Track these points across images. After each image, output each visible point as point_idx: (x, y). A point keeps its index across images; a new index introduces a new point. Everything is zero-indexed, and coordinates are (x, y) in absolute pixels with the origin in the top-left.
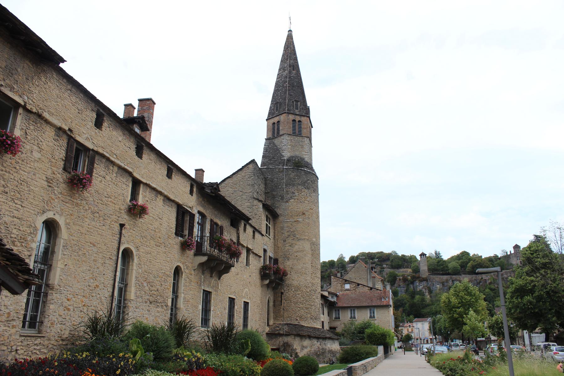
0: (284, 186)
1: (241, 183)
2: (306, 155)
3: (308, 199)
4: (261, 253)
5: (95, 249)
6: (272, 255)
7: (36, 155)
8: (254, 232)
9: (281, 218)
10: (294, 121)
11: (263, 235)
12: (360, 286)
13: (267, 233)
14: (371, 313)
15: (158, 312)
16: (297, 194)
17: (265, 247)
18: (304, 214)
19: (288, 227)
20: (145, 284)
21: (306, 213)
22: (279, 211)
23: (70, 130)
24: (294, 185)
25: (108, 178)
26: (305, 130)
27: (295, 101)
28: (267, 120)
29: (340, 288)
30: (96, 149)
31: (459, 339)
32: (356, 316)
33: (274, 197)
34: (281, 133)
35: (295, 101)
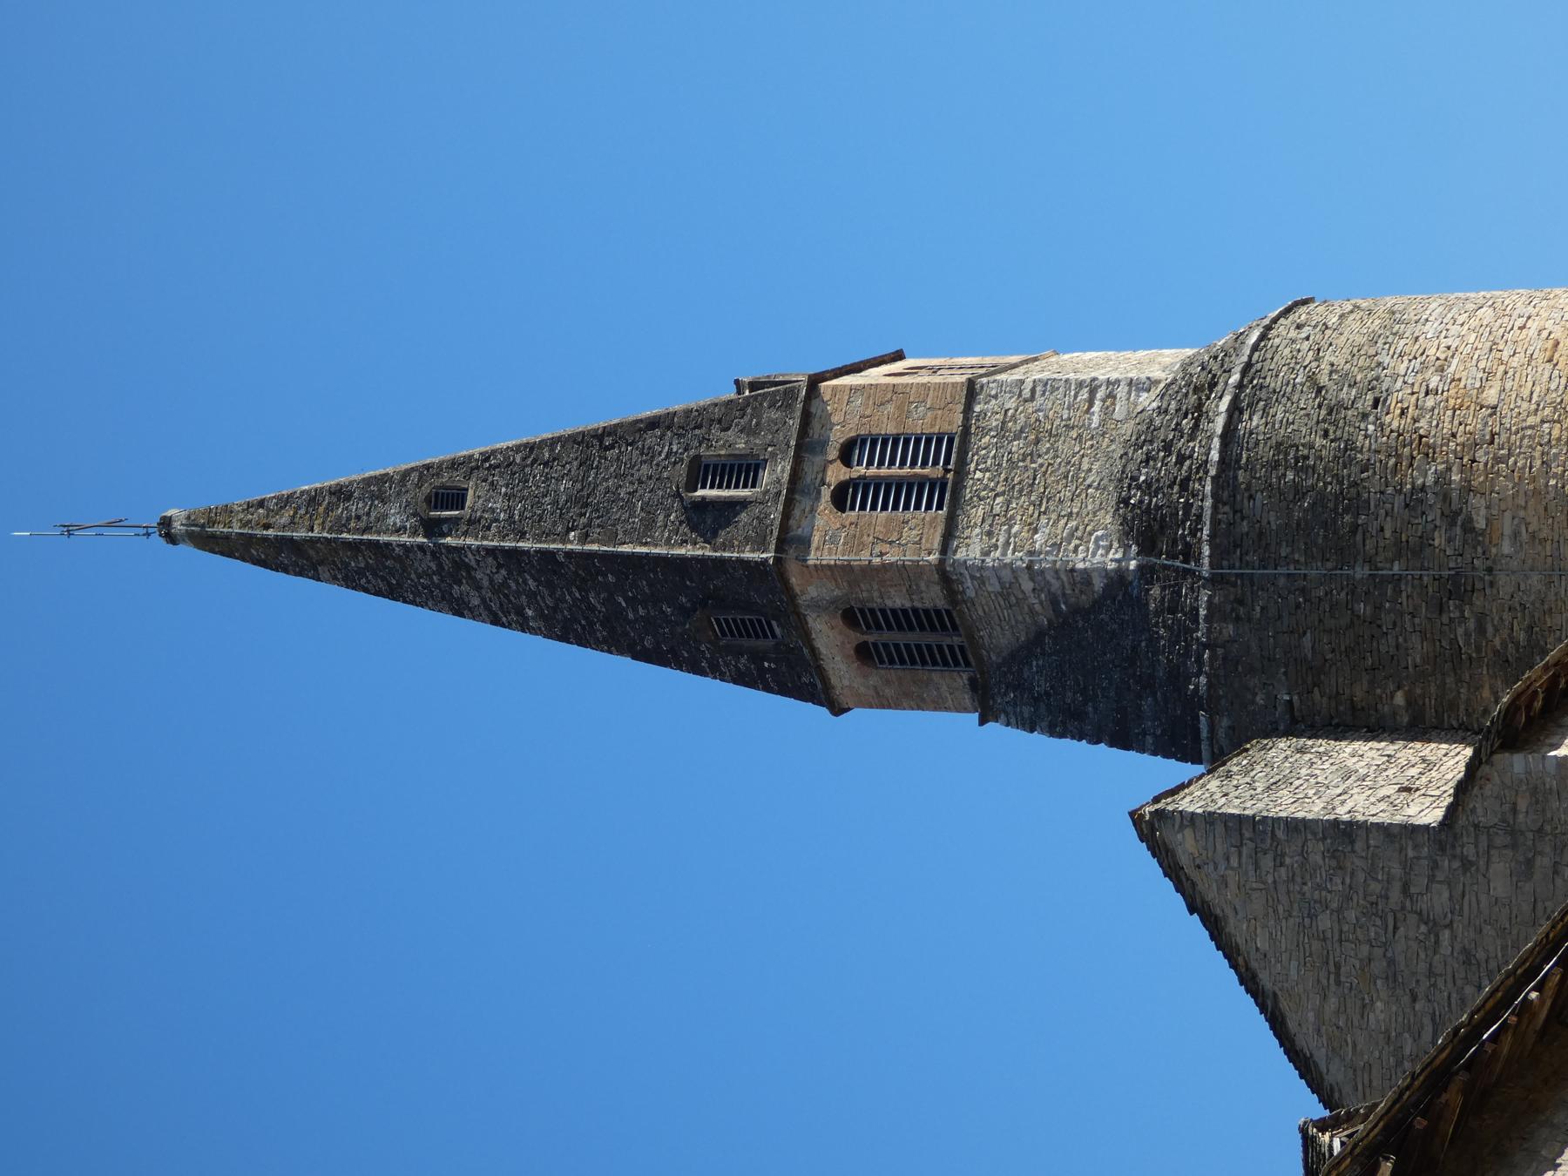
10: (841, 499)
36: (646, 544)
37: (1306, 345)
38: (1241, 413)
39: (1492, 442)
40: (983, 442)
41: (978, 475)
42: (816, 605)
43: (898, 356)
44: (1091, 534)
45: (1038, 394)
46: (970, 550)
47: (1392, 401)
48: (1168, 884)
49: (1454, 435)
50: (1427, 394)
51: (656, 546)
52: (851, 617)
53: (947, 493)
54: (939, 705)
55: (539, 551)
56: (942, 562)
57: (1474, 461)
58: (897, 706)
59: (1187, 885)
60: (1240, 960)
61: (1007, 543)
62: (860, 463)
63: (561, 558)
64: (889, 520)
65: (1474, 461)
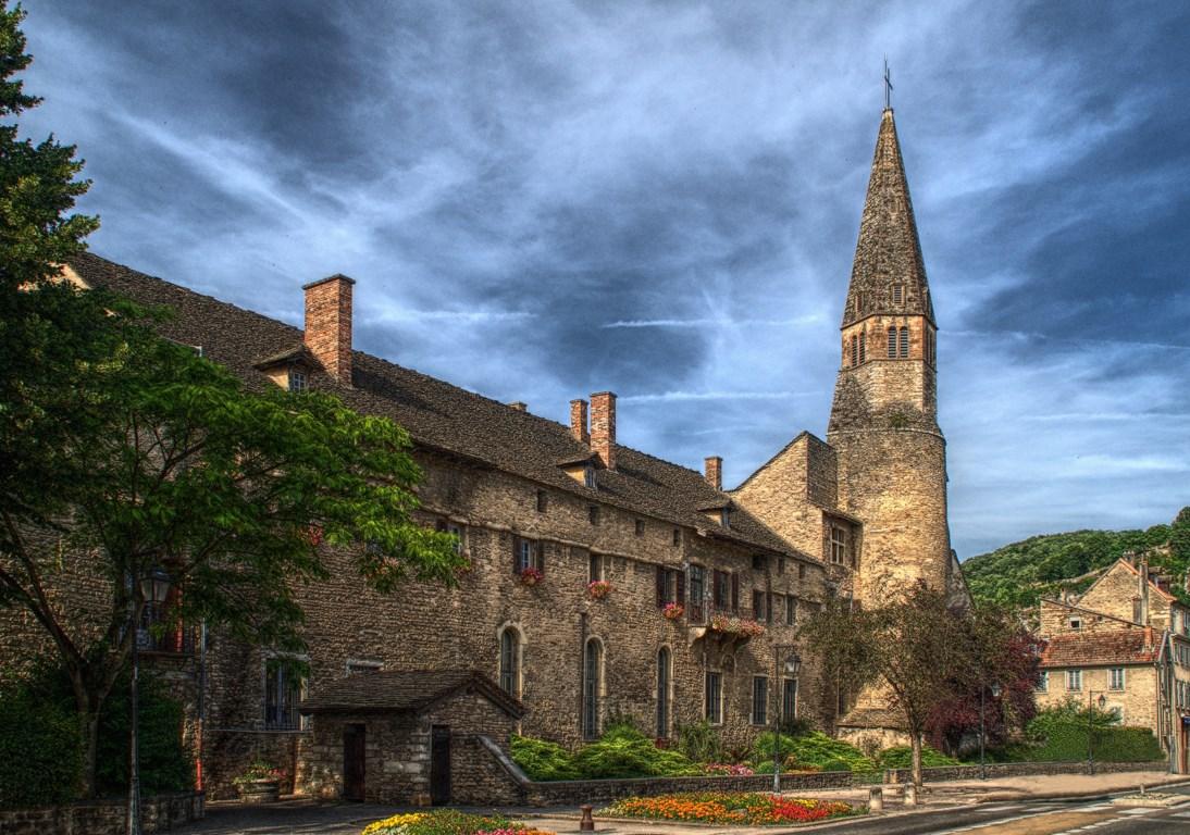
1: (786, 476)
5: (557, 648)
7: (488, 568)
8: (801, 567)
10: (892, 329)
12: (1104, 620)
13: (835, 559)
14: (1114, 679)
15: (640, 708)
19: (878, 542)
20: (620, 677)
23: (514, 528)
24: (888, 463)
25: (561, 564)
29: (1058, 626)
30: (543, 537)
32: (1081, 686)
34: (868, 357)
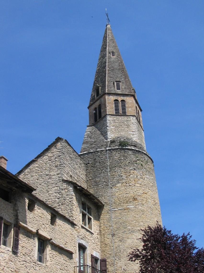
0: (108, 170)
2: (133, 135)
3: (140, 182)
4: (75, 249)
6: (97, 255)
9: (106, 208)
10: (116, 101)
11: (73, 224)
16: (124, 176)
17: (83, 242)
18: (135, 199)
21: (139, 198)
22: (103, 200)
26: (130, 109)
27: (116, 81)
28: (88, 108)
31: (72, 255)
33: (97, 184)
35: (116, 81)
36: (108, 77)
37: (144, 159)
38: (132, 151)
39: (130, 186)
40: (125, 118)
41: (121, 118)
42: (101, 100)
43: (141, 110)
44: (113, 134)
45: (134, 125)
46: (108, 118)
47: (135, 171)
48: (52, 142)
49: (130, 180)
50: (137, 176)
51: (107, 78)
52: (100, 106)
53: (117, 114)
54: (90, 120)
55: (106, 65)
56: (107, 115)
57: (126, 183)
58: (89, 115)
59: (52, 145)
60: (42, 154)
61: (111, 123)
62: (121, 103)
63: (106, 68)
64: (113, 107)
65: (126, 183)
